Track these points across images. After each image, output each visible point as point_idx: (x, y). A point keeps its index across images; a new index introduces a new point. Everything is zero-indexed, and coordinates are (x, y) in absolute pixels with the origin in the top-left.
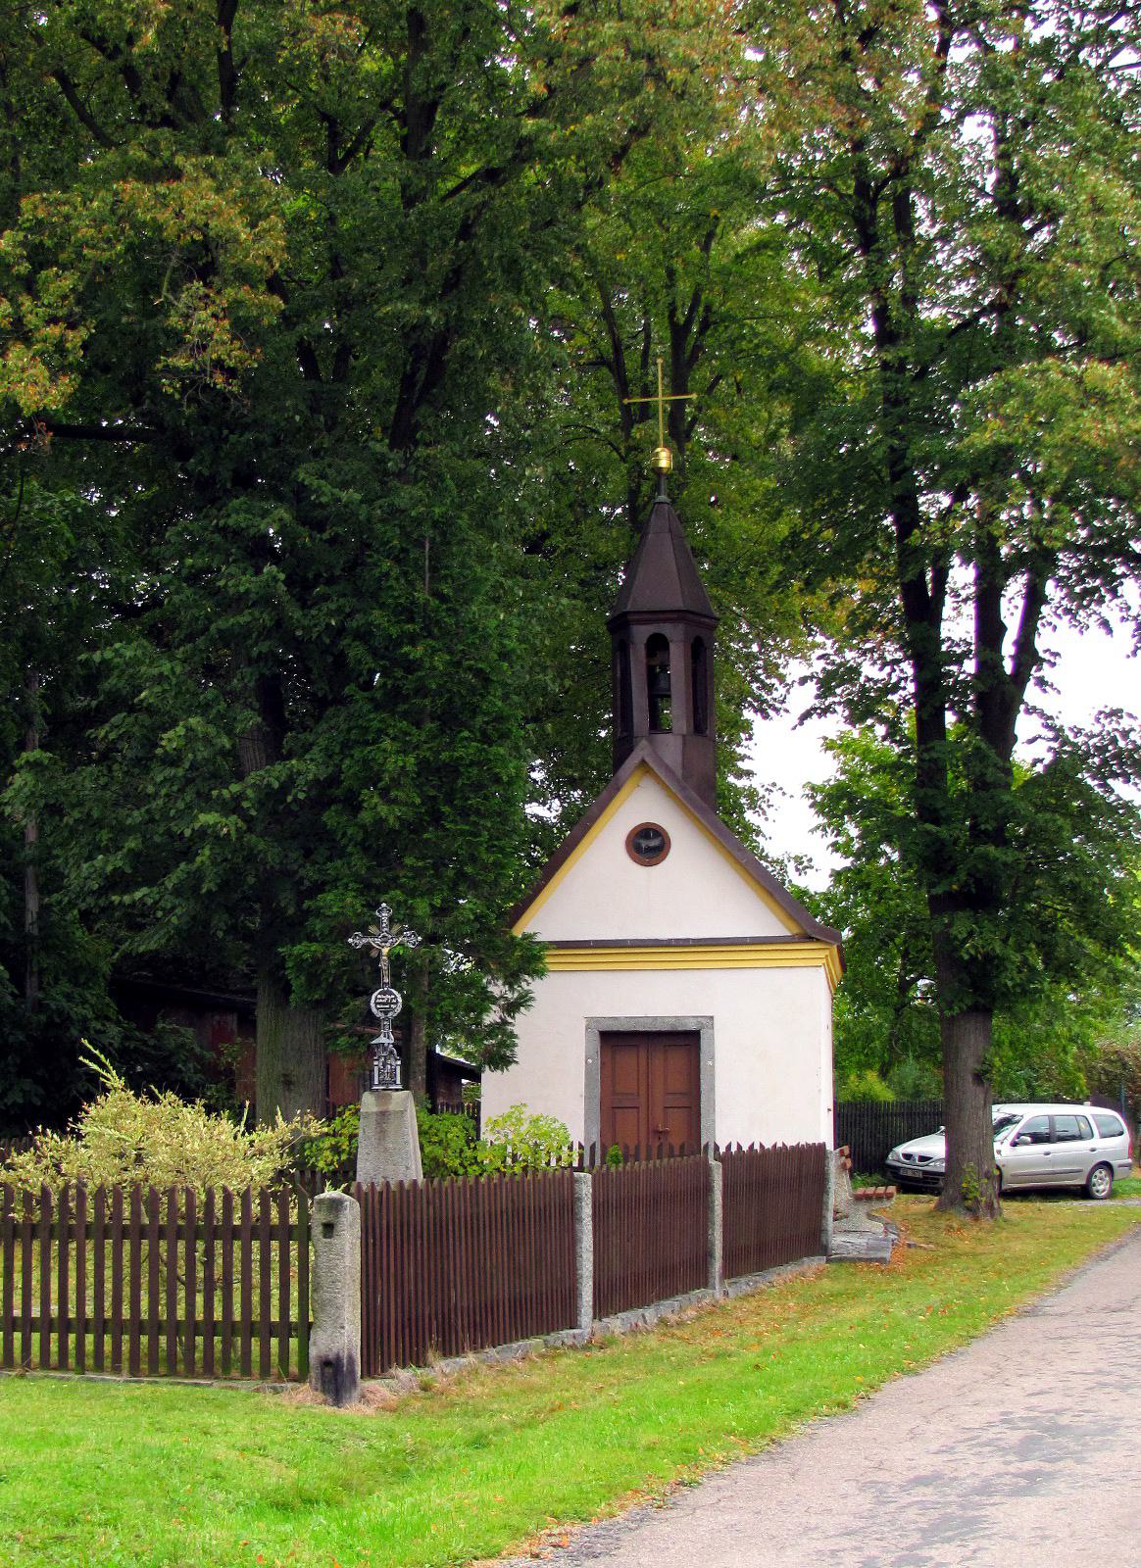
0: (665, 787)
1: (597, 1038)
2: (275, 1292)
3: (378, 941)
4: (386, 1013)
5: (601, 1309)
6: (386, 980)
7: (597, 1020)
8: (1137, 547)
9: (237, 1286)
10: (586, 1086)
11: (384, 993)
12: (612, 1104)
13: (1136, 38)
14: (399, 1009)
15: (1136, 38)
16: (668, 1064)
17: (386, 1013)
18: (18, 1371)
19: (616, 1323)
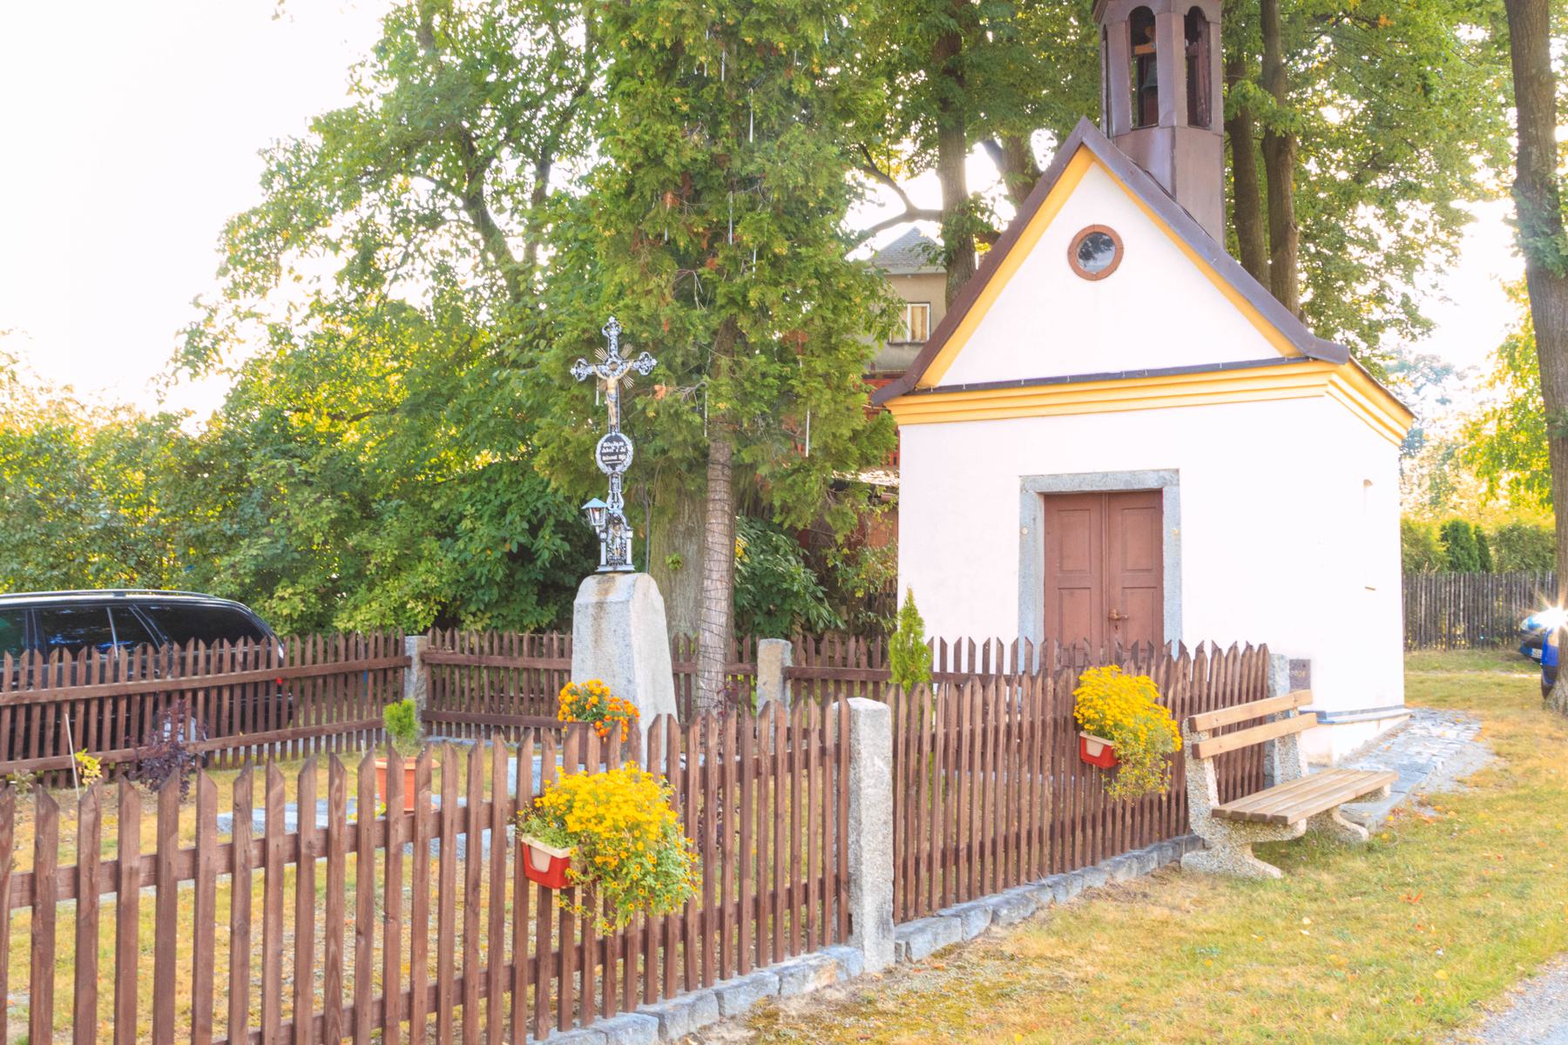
0: (1102, 165)
1: (1039, 507)
2: (105, 985)
3: (605, 369)
4: (613, 466)
5: (909, 905)
6: (614, 421)
7: (1035, 479)
8: (1553, 619)
9: (509, 904)
10: (1021, 561)
11: (610, 440)
12: (1058, 585)
13: (1538, 565)
14: (628, 460)
15: (1538, 565)
16: (1129, 521)
17: (613, 466)
18: (1156, 844)
19: (924, 939)
